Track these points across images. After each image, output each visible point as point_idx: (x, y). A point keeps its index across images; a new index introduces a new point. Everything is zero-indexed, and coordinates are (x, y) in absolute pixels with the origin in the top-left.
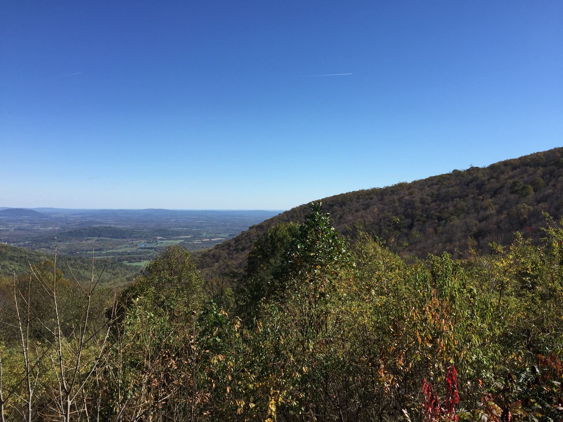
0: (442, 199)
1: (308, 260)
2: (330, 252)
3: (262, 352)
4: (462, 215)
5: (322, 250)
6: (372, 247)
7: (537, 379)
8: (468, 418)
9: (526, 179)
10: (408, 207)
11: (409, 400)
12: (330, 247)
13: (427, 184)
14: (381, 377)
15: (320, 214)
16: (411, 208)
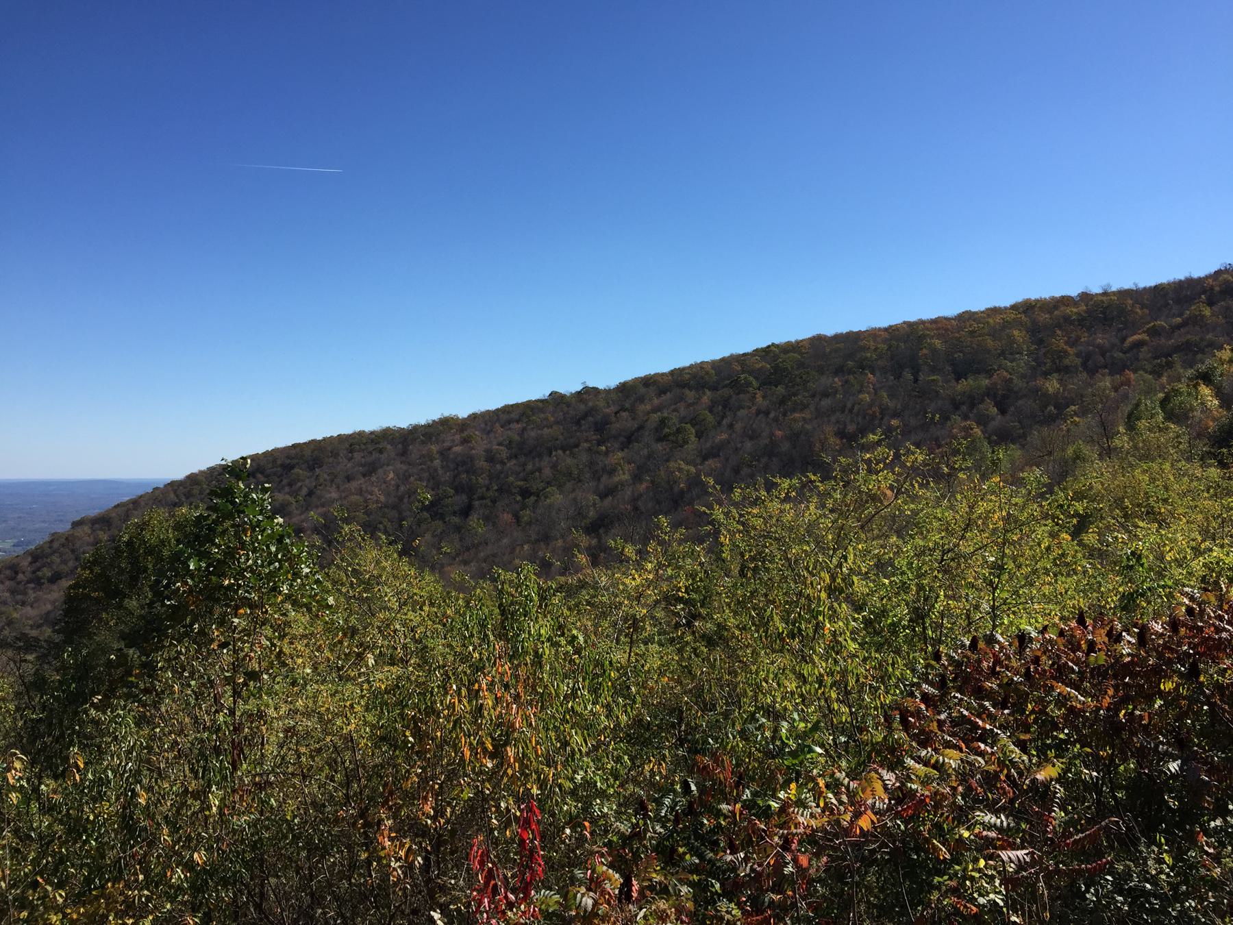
0: (530, 452)
1: (214, 596)
2: (271, 575)
3: (85, 831)
4: (569, 485)
5: (252, 572)
6: (376, 558)
7: (691, 804)
8: (556, 907)
9: (683, 411)
10: (460, 469)
11: (443, 889)
12: (270, 564)
13: (498, 420)
14: (384, 848)
15: (247, 486)
16: (467, 472)
